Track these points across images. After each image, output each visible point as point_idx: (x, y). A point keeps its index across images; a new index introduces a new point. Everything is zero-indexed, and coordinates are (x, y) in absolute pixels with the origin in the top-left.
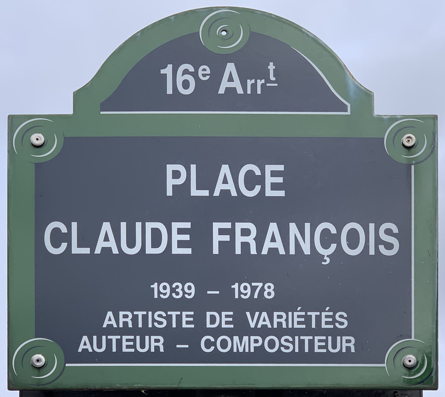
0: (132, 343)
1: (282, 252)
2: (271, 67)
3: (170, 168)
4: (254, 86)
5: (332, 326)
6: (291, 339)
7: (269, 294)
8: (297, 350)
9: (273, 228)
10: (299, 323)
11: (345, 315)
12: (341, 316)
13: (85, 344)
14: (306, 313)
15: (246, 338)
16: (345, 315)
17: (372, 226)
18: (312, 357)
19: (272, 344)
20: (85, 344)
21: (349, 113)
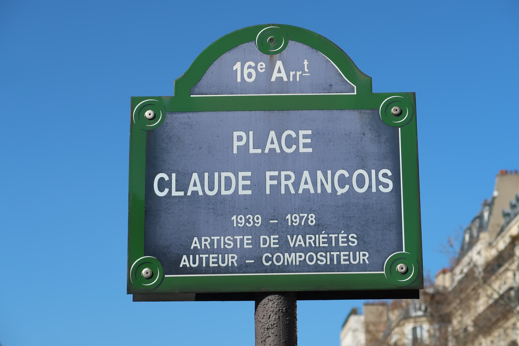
0: (347, 258)
1: (312, 191)
2: (306, 63)
3: (236, 134)
4: (295, 76)
5: (346, 245)
6: (324, 254)
7: (312, 222)
8: (328, 263)
9: (306, 174)
10: (323, 243)
11: (355, 236)
12: (353, 237)
13: (185, 261)
14: (328, 235)
15: (293, 255)
16: (355, 236)
17: (373, 172)
18: (208, 269)
19: (311, 259)
20: (185, 261)
21: (355, 93)
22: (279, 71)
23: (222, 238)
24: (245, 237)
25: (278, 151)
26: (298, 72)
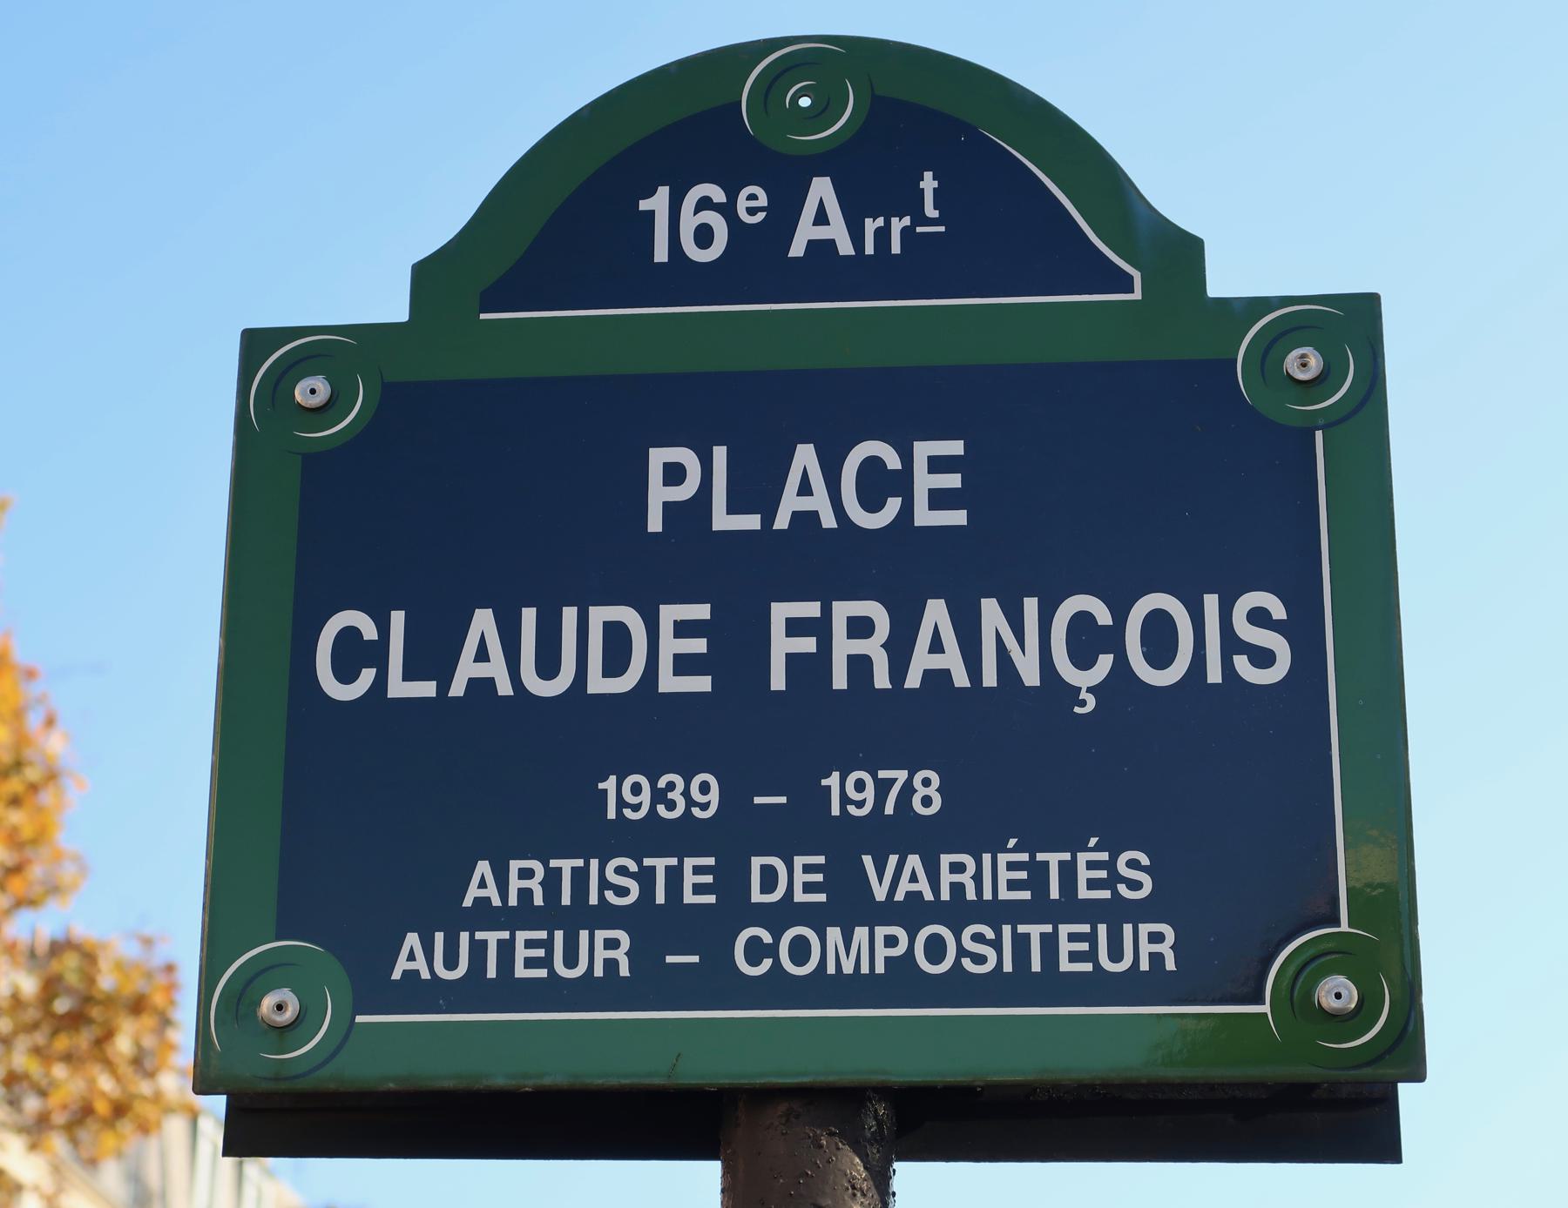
0: (540, 953)
2: (929, 183)
3: (659, 457)
4: (883, 235)
5: (1106, 894)
7: (927, 801)
8: (1008, 967)
9: (936, 613)
16: (1145, 860)
17: (1211, 602)
18: (510, 993)
21: (1137, 295)
22: (821, 218)
23: (594, 863)
24: (689, 863)
25: (829, 521)
26: (895, 220)
